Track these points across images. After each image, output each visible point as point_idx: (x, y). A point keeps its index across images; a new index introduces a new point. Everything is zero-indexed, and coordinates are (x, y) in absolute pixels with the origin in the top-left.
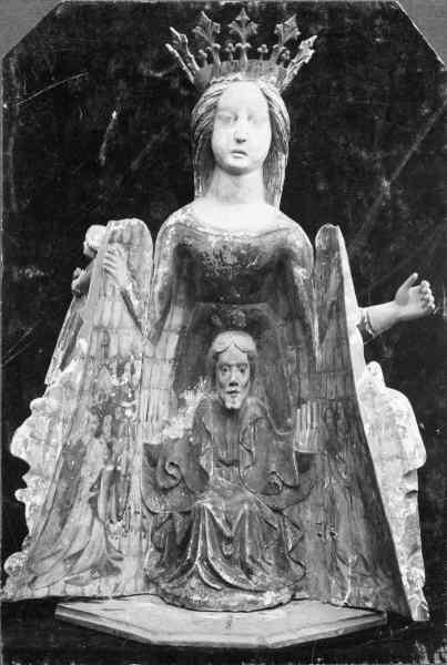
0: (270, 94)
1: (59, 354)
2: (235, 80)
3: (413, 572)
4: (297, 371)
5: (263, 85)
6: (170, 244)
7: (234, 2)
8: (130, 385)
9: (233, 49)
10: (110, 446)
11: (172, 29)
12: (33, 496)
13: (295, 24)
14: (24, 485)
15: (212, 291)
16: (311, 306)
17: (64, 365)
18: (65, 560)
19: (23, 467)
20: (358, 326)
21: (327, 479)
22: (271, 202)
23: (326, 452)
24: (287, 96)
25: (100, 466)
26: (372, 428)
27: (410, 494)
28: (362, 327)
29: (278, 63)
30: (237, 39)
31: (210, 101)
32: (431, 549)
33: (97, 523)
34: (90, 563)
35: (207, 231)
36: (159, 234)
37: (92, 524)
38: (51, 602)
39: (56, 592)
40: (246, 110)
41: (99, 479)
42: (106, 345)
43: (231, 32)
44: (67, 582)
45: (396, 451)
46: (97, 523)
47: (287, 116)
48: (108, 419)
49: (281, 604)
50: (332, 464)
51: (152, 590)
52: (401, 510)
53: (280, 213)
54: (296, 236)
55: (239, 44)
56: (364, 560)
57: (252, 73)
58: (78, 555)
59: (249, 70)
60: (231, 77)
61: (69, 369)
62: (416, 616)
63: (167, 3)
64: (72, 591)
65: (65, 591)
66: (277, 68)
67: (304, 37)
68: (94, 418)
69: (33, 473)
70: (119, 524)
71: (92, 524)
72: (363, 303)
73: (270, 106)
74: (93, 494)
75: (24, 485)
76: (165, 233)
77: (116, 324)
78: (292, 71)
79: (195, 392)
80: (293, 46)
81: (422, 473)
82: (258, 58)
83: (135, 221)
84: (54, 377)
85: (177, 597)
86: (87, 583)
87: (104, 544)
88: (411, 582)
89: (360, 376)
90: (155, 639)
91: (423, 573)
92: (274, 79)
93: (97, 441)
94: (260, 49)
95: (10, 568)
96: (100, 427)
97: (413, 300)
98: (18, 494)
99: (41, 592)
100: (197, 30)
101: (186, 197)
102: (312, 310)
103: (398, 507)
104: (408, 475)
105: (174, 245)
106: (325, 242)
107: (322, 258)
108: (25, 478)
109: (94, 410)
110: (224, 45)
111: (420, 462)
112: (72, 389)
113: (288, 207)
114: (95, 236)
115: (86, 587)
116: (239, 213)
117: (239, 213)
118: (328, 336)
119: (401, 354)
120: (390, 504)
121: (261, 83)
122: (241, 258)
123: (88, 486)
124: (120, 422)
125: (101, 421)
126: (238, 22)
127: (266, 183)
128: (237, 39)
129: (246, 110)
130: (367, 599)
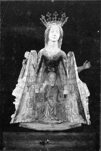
0: (60, 27)
1: (21, 76)
2: (54, 24)
3: (88, 117)
4: (63, 79)
5: (59, 26)
6: (41, 55)
7: (22, 1)
8: (33, 82)
9: (54, 19)
10: (30, 93)
11: (42, 15)
12: (16, 103)
13: (65, 14)
14: (15, 101)
15: (51, 65)
16: (67, 67)
17: (22, 77)
18: (21, 116)
19: (15, 97)
20: (77, 70)
21: (70, 99)
22: (59, 48)
23: (70, 94)
24: (63, 27)
25: (28, 97)
26: (80, 89)
27: (87, 101)
28: (78, 70)
29: (62, 22)
30: (54, 17)
31: (49, 28)
32: (90, 113)
33: (27, 108)
34: (26, 116)
35: (48, 53)
36: (39, 53)
37: (27, 108)
38: (19, 123)
39: (20, 122)
40: (54, 31)
41: (28, 99)
42: (30, 74)
43: (53, 15)
44: (22, 120)
45: (84, 93)
46: (27, 108)
47: (63, 31)
48: (30, 88)
49: (62, 123)
50: (71, 96)
51: (37, 121)
52: (86, 104)
53: (45, 47)
54: (64, 53)
55: (55, 18)
56: (77, 114)
57: (57, 24)
58: (24, 114)
59: (56, 22)
60: (53, 24)
61: (23, 79)
62: (88, 124)
63: (8, 2)
64: (23, 121)
65: (21, 122)
66: (61, 23)
67: (66, 17)
68: (27, 88)
69: (17, 99)
70: (31, 108)
71: (27, 108)
72: (78, 66)
73: (60, 29)
74: (27, 103)
75: (15, 101)
76: (40, 53)
77: (31, 70)
78: (64, 23)
79: (45, 83)
80: (64, 19)
81: (89, 97)
82: (58, 20)
83: (35, 51)
84: (20, 80)
85: (42, 122)
86: (25, 120)
87: (29, 112)
88: (87, 118)
89: (77, 79)
90: (37, 130)
91: (89, 116)
92: (61, 24)
93: (27, 92)
94: (59, 19)
95: (12, 117)
96: (28, 90)
97: (87, 66)
98: (14, 103)
99: (17, 122)
100: (47, 15)
101: (43, 46)
102: (67, 68)
103: (85, 104)
104: (86, 98)
105: (41, 55)
106: (69, 55)
107: (71, 59)
108: (15, 100)
109: (28, 87)
110: (52, 18)
111: (89, 95)
112: (24, 82)
113: (62, 49)
114: (27, 54)
115: (25, 120)
116: (52, 49)
117: (52, 49)
118: (70, 72)
119: (83, 76)
120: (84, 103)
121: (58, 25)
122: (54, 58)
123: (26, 101)
124: (31, 89)
125: (28, 88)
126: (55, 13)
127: (58, 44)
128: (54, 17)
129: (54, 31)
130: (78, 121)
